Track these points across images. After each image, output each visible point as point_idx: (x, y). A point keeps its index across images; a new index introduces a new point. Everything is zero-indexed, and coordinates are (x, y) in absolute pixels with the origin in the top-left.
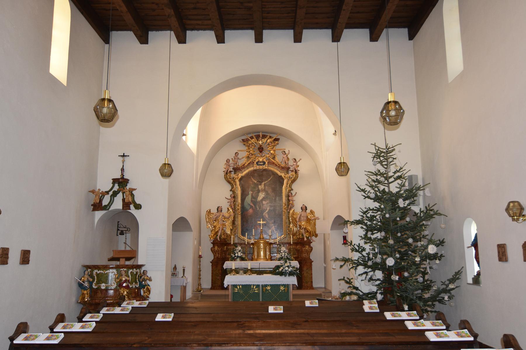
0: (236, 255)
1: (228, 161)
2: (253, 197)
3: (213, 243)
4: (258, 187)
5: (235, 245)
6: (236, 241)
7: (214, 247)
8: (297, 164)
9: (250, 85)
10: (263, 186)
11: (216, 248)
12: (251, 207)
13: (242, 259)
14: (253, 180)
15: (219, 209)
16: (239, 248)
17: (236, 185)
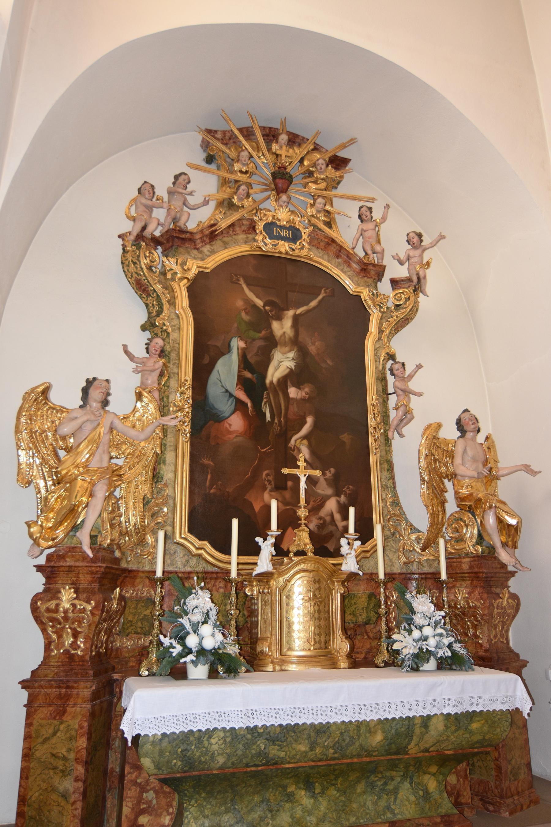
0: (192, 641)
1: (146, 190)
2: (245, 362)
3: (50, 571)
4: (269, 327)
5: (180, 584)
6: (180, 564)
7: (50, 592)
8: (421, 256)
9: (222, 24)
10: (288, 323)
11: (67, 597)
12: (240, 405)
13: (221, 666)
14: (251, 295)
15: (95, 394)
16: (201, 601)
17: (172, 303)
